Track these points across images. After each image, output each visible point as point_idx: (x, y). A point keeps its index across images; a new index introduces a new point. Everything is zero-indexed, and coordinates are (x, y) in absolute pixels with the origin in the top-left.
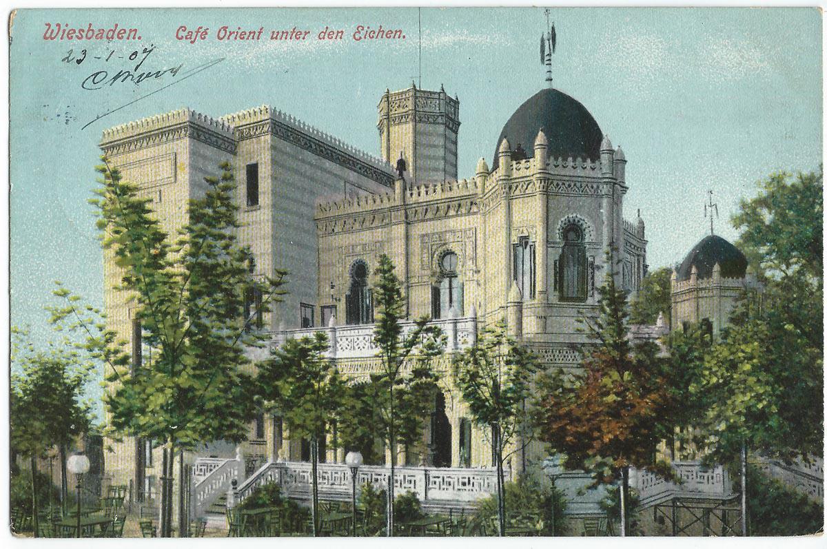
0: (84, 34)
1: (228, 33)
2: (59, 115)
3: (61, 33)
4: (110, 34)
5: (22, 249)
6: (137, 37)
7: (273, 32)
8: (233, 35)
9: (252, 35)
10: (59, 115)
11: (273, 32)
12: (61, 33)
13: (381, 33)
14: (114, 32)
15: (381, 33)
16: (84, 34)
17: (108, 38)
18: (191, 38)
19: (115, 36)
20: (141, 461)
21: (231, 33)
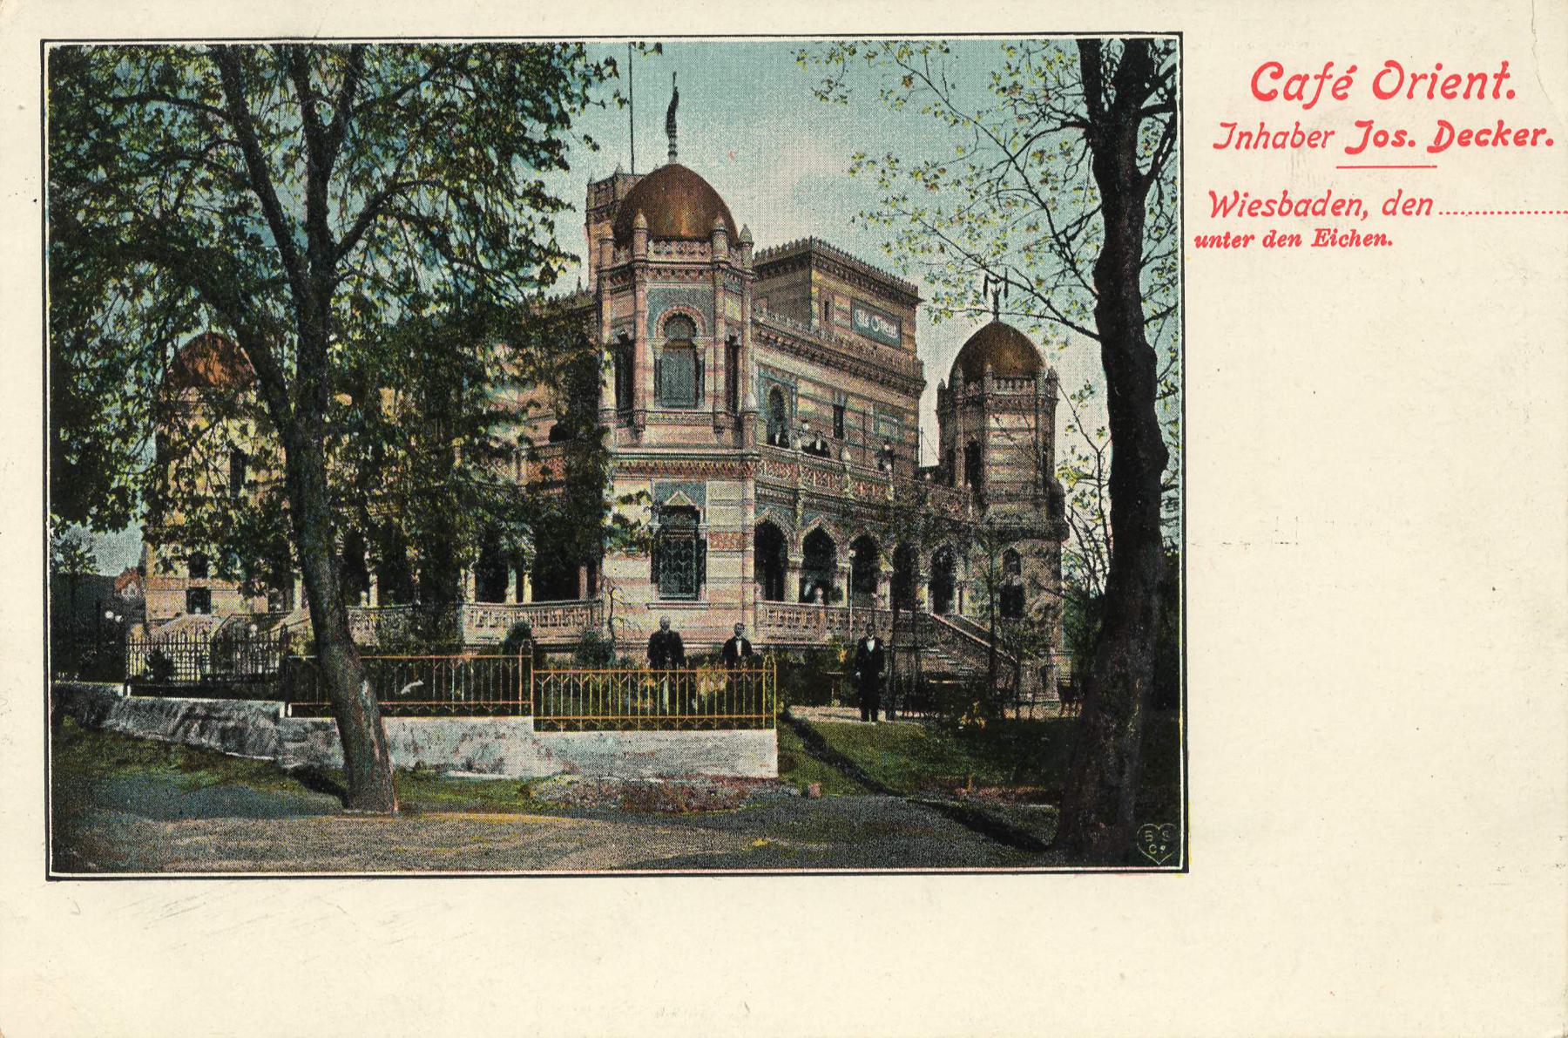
0: (1276, 207)
1: (1408, 81)
2: (1122, 976)
3: (1239, 203)
4: (1279, 140)
5: (1159, 843)
6: (1503, 91)
7: (1428, 213)
8: (1423, 85)
9: (1245, 139)
10: (1122, 976)
11: (1428, 213)
12: (1239, 203)
13: (1263, 138)
14: (1397, 202)
15: (1263, 138)
16: (1276, 207)
17: (1275, 146)
18: (1299, 95)
19: (1399, 210)
20: (1005, 407)
21: (1415, 78)
